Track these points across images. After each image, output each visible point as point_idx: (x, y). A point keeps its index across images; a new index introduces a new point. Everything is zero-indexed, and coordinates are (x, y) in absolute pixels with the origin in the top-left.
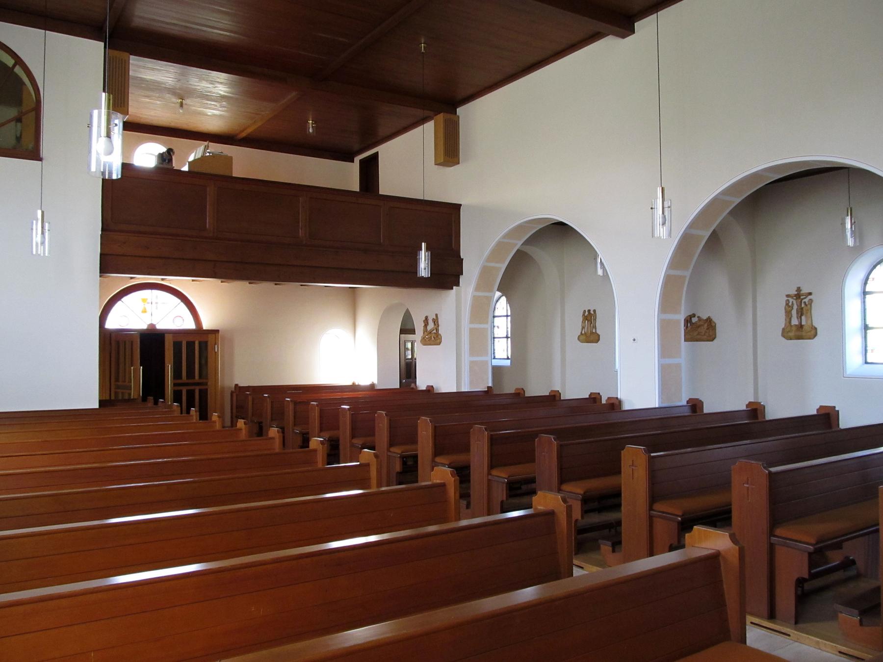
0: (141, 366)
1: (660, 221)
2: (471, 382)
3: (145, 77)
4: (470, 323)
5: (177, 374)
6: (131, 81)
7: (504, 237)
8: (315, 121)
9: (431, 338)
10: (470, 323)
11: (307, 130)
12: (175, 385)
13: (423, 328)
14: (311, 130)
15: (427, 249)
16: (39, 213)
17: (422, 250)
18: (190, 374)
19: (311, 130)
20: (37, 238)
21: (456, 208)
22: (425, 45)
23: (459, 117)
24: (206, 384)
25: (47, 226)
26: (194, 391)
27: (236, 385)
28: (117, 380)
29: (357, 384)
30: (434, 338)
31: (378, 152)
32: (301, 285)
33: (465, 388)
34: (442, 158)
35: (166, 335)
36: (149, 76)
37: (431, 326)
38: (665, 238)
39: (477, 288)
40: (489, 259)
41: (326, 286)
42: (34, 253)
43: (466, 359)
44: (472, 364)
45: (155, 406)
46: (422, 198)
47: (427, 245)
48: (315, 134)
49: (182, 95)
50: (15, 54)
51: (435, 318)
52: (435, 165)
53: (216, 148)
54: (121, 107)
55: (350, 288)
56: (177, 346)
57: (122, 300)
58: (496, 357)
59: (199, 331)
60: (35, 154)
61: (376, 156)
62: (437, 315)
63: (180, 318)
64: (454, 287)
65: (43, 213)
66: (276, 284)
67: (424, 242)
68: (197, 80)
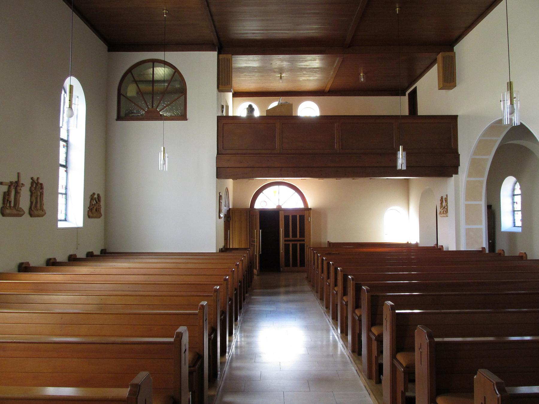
0: (260, 229)
1: (507, 111)
2: (467, 244)
3: (242, 65)
4: (466, 201)
5: (286, 234)
6: (233, 70)
7: (484, 135)
8: (365, 73)
9: (444, 212)
10: (466, 201)
11: (360, 80)
12: (285, 241)
13: (440, 205)
14: (362, 80)
15: (404, 150)
16: (162, 148)
17: (399, 151)
18: (295, 235)
19: (362, 80)
20: (161, 162)
21: (454, 119)
22: (399, 9)
23: (455, 53)
24: (304, 240)
25: (166, 155)
26: (296, 245)
27: (328, 242)
28: (252, 238)
29: (409, 243)
30: (446, 212)
31: (416, 86)
32: (370, 179)
33: (463, 248)
34: (442, 84)
35: (280, 211)
36: (244, 65)
37: (444, 204)
38: (506, 123)
39: (470, 175)
40: (475, 153)
41: (387, 179)
42: (160, 169)
43: (463, 226)
44: (468, 230)
45: (69, 262)
46: (399, 114)
47: (403, 147)
48: (365, 82)
49: (263, 71)
50: (175, 67)
51: (446, 197)
52: (439, 89)
53: (283, 100)
54: (451, 83)
55: (405, 179)
56: (286, 218)
57: (263, 192)
58: (516, 225)
59: (307, 209)
60: (185, 119)
61: (416, 88)
62: (447, 195)
63: (265, 202)
64: (453, 175)
65: (164, 148)
66: (353, 179)
67: (401, 145)
68: (280, 61)
